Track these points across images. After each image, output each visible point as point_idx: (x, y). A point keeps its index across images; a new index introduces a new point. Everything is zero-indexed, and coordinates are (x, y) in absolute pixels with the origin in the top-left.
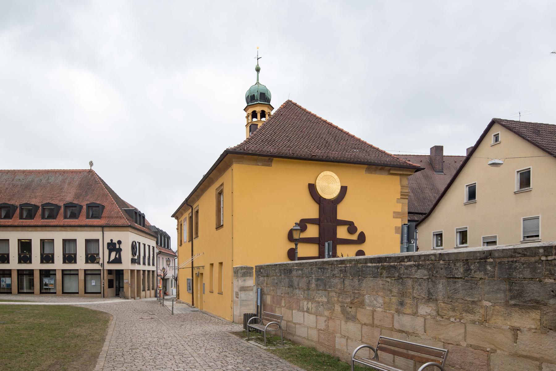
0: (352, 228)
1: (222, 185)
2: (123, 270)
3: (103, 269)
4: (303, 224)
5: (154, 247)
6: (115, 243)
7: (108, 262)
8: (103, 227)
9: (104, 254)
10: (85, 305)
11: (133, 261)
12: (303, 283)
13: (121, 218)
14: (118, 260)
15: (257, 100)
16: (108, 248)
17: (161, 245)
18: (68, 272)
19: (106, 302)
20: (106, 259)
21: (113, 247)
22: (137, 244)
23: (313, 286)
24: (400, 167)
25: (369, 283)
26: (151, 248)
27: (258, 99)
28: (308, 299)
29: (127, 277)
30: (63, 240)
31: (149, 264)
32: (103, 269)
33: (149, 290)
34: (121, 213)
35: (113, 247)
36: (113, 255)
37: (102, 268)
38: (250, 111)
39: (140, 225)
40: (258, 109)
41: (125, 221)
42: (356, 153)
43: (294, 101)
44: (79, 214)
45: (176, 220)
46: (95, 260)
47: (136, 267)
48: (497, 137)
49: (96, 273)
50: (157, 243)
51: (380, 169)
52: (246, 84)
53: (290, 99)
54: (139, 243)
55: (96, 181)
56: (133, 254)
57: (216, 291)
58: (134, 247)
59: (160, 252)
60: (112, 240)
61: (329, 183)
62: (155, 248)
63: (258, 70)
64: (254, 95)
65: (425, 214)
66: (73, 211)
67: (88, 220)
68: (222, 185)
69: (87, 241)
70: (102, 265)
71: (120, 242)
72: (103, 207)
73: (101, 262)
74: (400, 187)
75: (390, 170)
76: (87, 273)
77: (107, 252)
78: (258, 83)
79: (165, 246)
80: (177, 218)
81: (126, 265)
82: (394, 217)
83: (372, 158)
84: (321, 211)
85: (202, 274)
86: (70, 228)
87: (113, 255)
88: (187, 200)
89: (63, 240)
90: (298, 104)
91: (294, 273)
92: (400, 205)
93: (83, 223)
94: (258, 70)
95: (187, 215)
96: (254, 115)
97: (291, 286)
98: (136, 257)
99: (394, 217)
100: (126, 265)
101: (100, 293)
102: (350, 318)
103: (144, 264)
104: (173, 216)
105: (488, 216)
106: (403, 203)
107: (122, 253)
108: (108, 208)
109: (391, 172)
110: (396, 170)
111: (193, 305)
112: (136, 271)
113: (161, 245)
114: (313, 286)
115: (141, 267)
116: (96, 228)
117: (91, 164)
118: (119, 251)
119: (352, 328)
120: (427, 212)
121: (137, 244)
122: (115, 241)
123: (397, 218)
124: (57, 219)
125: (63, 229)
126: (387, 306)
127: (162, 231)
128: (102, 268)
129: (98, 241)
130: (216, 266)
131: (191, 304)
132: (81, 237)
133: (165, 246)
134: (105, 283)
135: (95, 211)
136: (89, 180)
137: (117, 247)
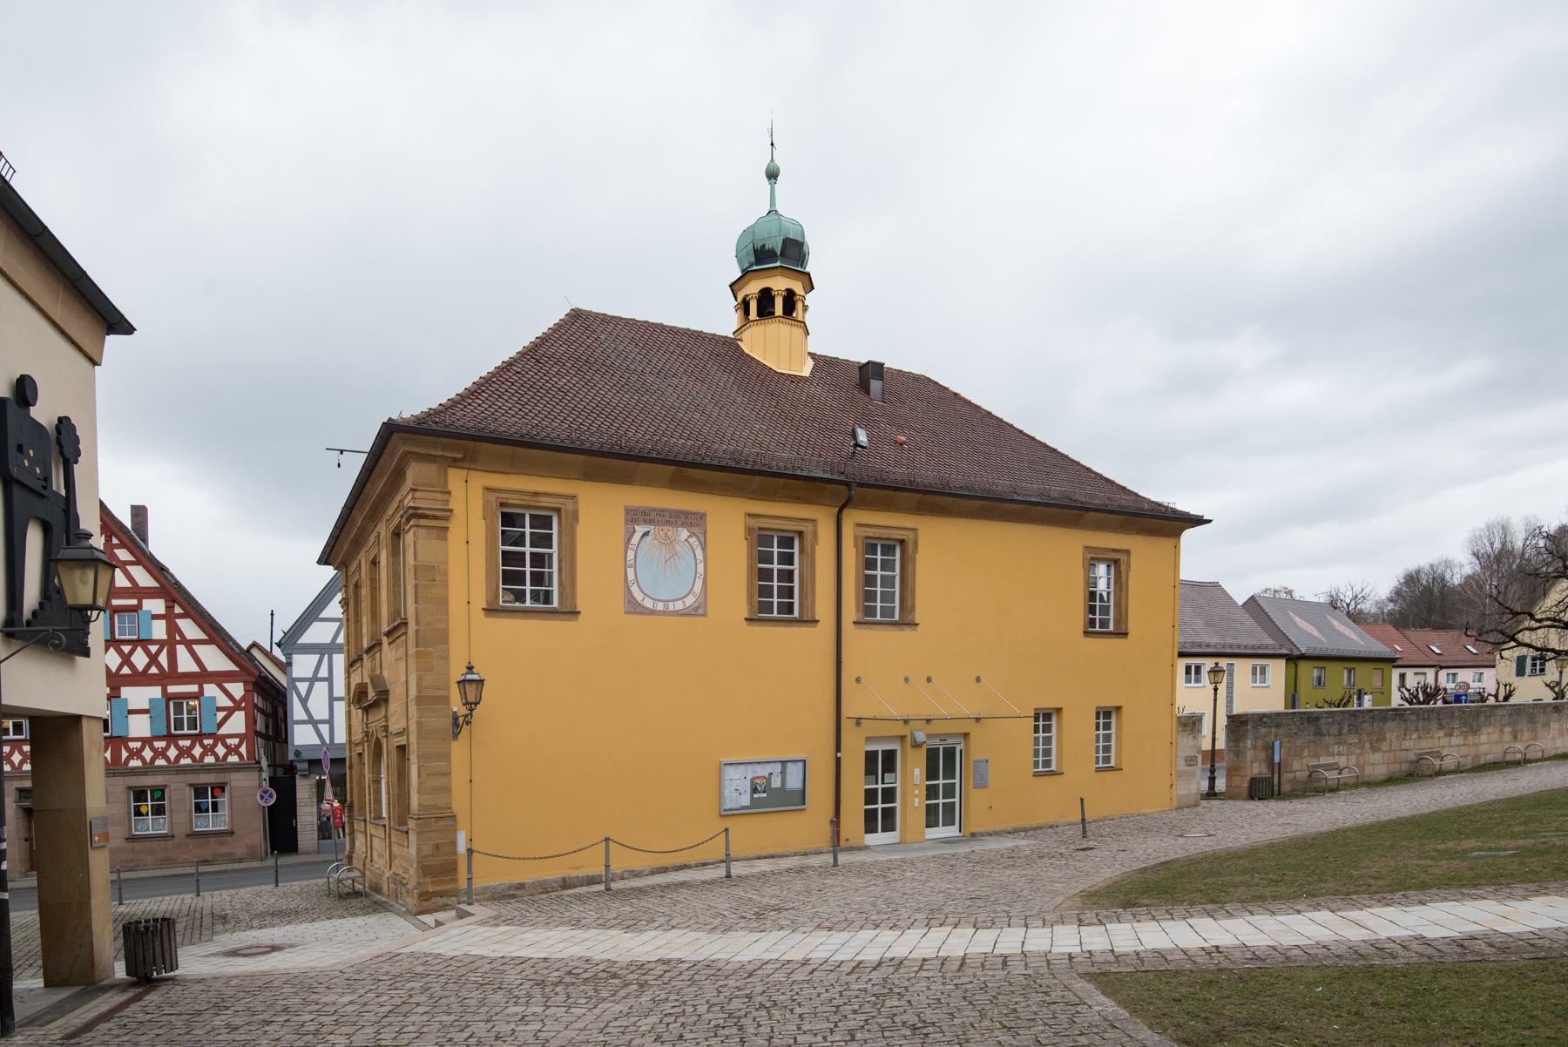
12: (1334, 729)
23: (1345, 730)
25: (1390, 724)
28: (1339, 743)
52: (741, 210)
63: (772, 175)
91: (1323, 721)
94: (772, 175)
97: (1318, 733)
101: (800, 798)
102: (1374, 750)
114: (1345, 730)
119: (1378, 757)
126: (1398, 738)
130: (1077, 731)
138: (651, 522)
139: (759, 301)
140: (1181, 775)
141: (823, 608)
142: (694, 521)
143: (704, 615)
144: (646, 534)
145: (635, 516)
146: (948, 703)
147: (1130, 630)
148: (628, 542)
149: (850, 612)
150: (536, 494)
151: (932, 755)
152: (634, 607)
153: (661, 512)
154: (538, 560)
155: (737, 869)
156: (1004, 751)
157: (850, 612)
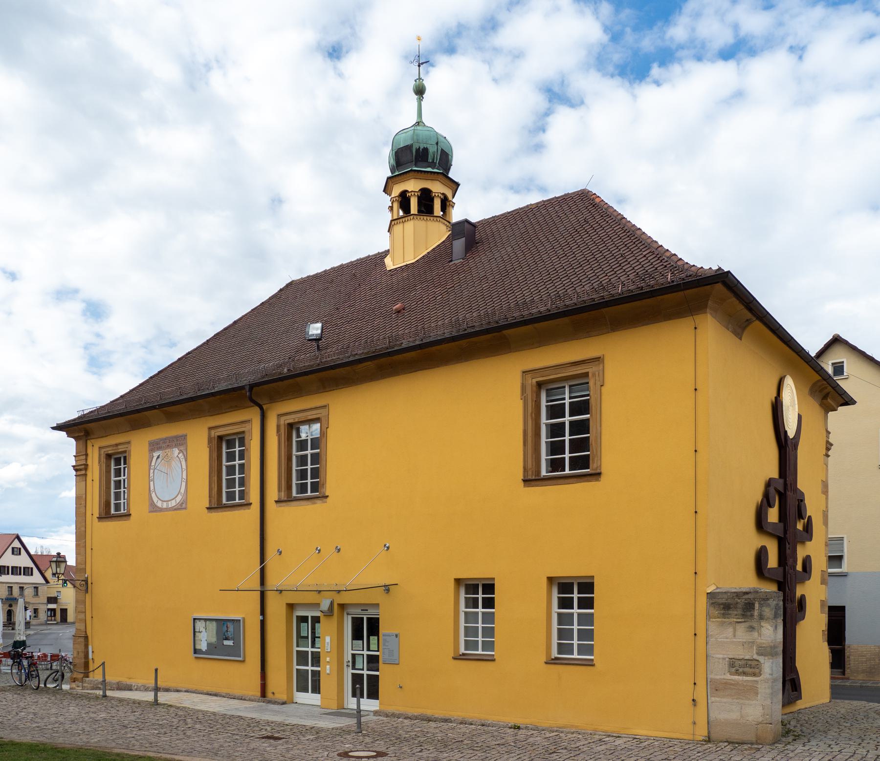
130: (526, 611)
138: (159, 449)
139: (419, 198)
140: (716, 688)
141: (254, 496)
142: (179, 441)
143: (185, 508)
144: (158, 457)
145: (155, 446)
146: (357, 573)
147: (604, 470)
148: (150, 465)
149: (273, 493)
150: (117, 445)
151: (357, 624)
152: (154, 508)
153: (164, 440)
154: (242, 466)
155: (163, 697)
156: (425, 624)
157: (273, 493)
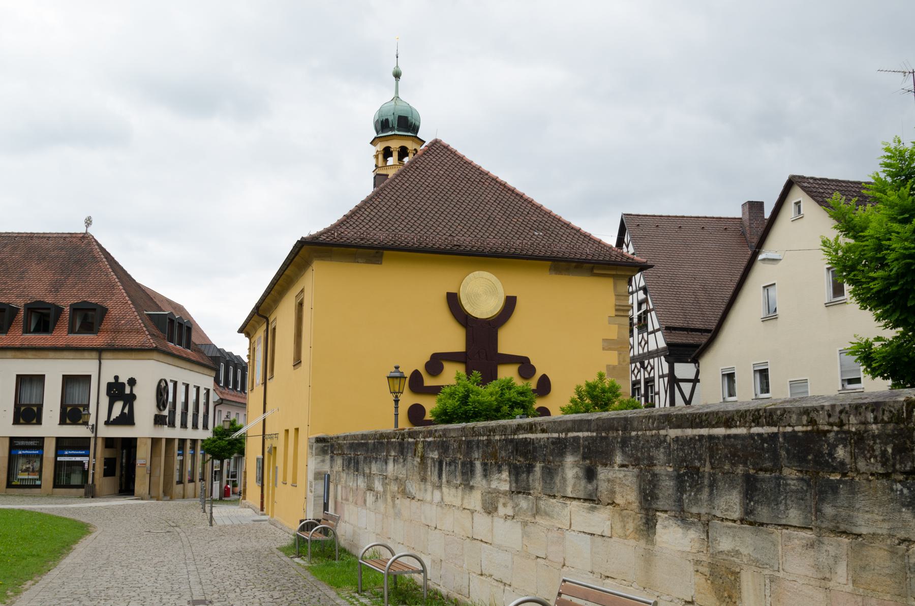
0: (525, 367)
1: (302, 291)
2: (136, 439)
3: (96, 437)
4: (436, 364)
5: (208, 391)
6: (123, 384)
7: (107, 423)
8: (100, 352)
9: (99, 406)
10: (49, 509)
11: (159, 420)
13: (138, 331)
14: (127, 419)
15: (392, 129)
16: (108, 394)
17: (227, 383)
18: (22, 443)
19: (58, 506)
20: (103, 417)
21: (119, 391)
22: (171, 386)
24: (609, 264)
26: (203, 392)
27: (396, 127)
29: (143, 454)
30: (18, 376)
31: (195, 426)
32: (96, 437)
33: (203, 479)
34: (139, 324)
35: (119, 391)
36: (118, 407)
37: (92, 435)
38: (380, 147)
39: (180, 344)
40: (395, 145)
41: (146, 339)
42: (537, 240)
43: (446, 141)
44: (55, 324)
45: (247, 340)
46: (80, 418)
47: (165, 432)
48: (798, 204)
49: (81, 444)
50: (217, 381)
51: (576, 267)
53: (439, 138)
54: (175, 383)
55: (94, 257)
56: (158, 406)
57: (289, 481)
58: (161, 392)
59: (222, 399)
60: (116, 378)
61: (483, 292)
62: (211, 392)
63: (397, 75)
64: (387, 120)
65: (708, 331)
66: (42, 318)
67: (71, 336)
68: (302, 291)
69: (68, 380)
70: (95, 428)
71: (132, 382)
72: (104, 311)
73: (92, 421)
74: (613, 298)
75: (592, 269)
76: (62, 444)
77: (105, 400)
78: (397, 97)
79: (235, 387)
80: (248, 335)
81: (143, 428)
82: (604, 349)
83: (561, 248)
84: (470, 340)
85: (275, 448)
86: (34, 353)
87: (118, 407)
88: (257, 308)
89: (18, 376)
90: (346, 212)
92: (615, 328)
93: (61, 343)
94: (397, 75)
95: (260, 333)
96: (387, 153)
98: (166, 413)
99: (604, 349)
100: (143, 428)
103: (184, 425)
104: (241, 331)
105: (800, 337)
106: (619, 325)
107: (137, 405)
108: (114, 312)
109: (595, 271)
110: (605, 269)
111: (262, 509)
112: (164, 442)
113: (227, 383)
115: (176, 433)
116: (86, 354)
117: (88, 222)
118: (130, 399)
120: (713, 327)
121: (171, 386)
122: (123, 379)
123: (610, 349)
124: (10, 334)
125: (18, 354)
127: (230, 354)
128: (92, 435)
129: (88, 378)
130: (292, 433)
131: (259, 507)
132: (54, 370)
133: (235, 387)
134: (97, 466)
135: (89, 317)
136: (79, 253)
137: (127, 391)
